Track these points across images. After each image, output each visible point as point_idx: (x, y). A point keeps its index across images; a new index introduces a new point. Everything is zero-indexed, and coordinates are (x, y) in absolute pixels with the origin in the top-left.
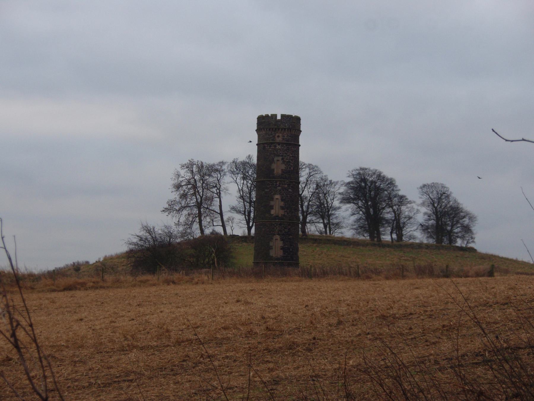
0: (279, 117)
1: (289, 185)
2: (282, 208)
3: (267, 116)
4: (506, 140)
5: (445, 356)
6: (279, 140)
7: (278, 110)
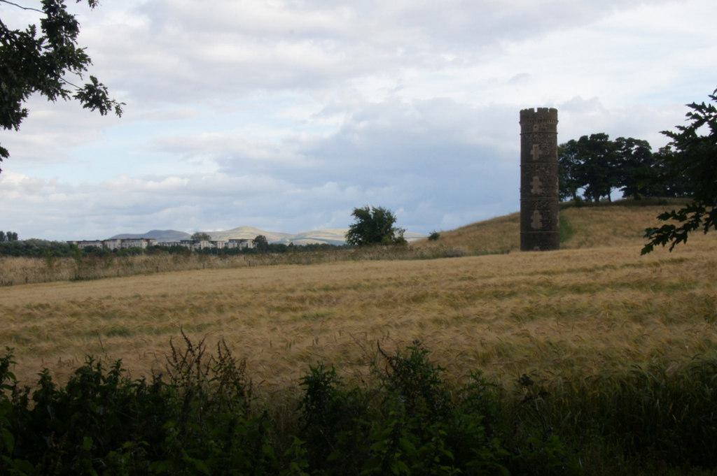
0: (536, 111)
1: (546, 167)
2: (541, 187)
3: (526, 110)
4: (25, 9)
5: (421, 273)
6: (535, 130)
7: (535, 103)
